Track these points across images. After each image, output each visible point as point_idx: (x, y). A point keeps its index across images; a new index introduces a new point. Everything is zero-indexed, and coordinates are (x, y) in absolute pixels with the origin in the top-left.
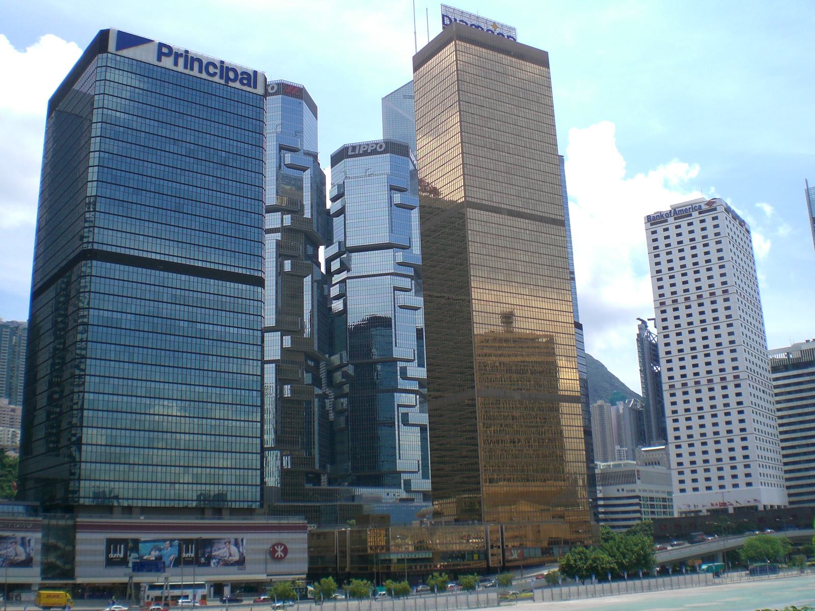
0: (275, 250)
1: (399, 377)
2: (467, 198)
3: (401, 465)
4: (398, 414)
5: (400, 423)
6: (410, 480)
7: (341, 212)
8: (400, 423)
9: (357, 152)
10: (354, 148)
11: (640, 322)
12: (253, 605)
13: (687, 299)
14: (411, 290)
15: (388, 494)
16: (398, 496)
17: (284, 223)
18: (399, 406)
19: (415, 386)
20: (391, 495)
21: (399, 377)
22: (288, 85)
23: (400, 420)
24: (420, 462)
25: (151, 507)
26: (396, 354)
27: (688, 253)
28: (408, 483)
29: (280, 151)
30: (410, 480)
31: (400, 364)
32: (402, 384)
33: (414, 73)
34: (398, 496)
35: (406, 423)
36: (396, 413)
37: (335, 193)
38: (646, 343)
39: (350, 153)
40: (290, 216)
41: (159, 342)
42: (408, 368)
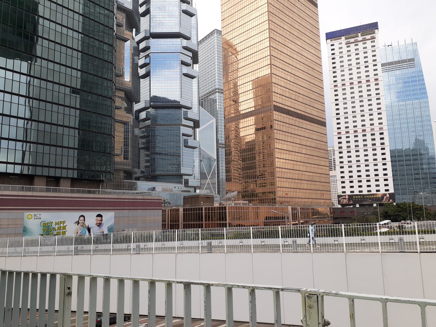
7: (147, 12)
12: (23, 150)
13: (355, 131)
14: (192, 136)
15: (175, 188)
18: (183, 135)
20: (177, 188)
25: (14, 174)
26: (183, 171)
27: (357, 104)
28: (187, 182)
30: (188, 180)
31: (183, 110)
41: (65, 159)
42: (189, 180)
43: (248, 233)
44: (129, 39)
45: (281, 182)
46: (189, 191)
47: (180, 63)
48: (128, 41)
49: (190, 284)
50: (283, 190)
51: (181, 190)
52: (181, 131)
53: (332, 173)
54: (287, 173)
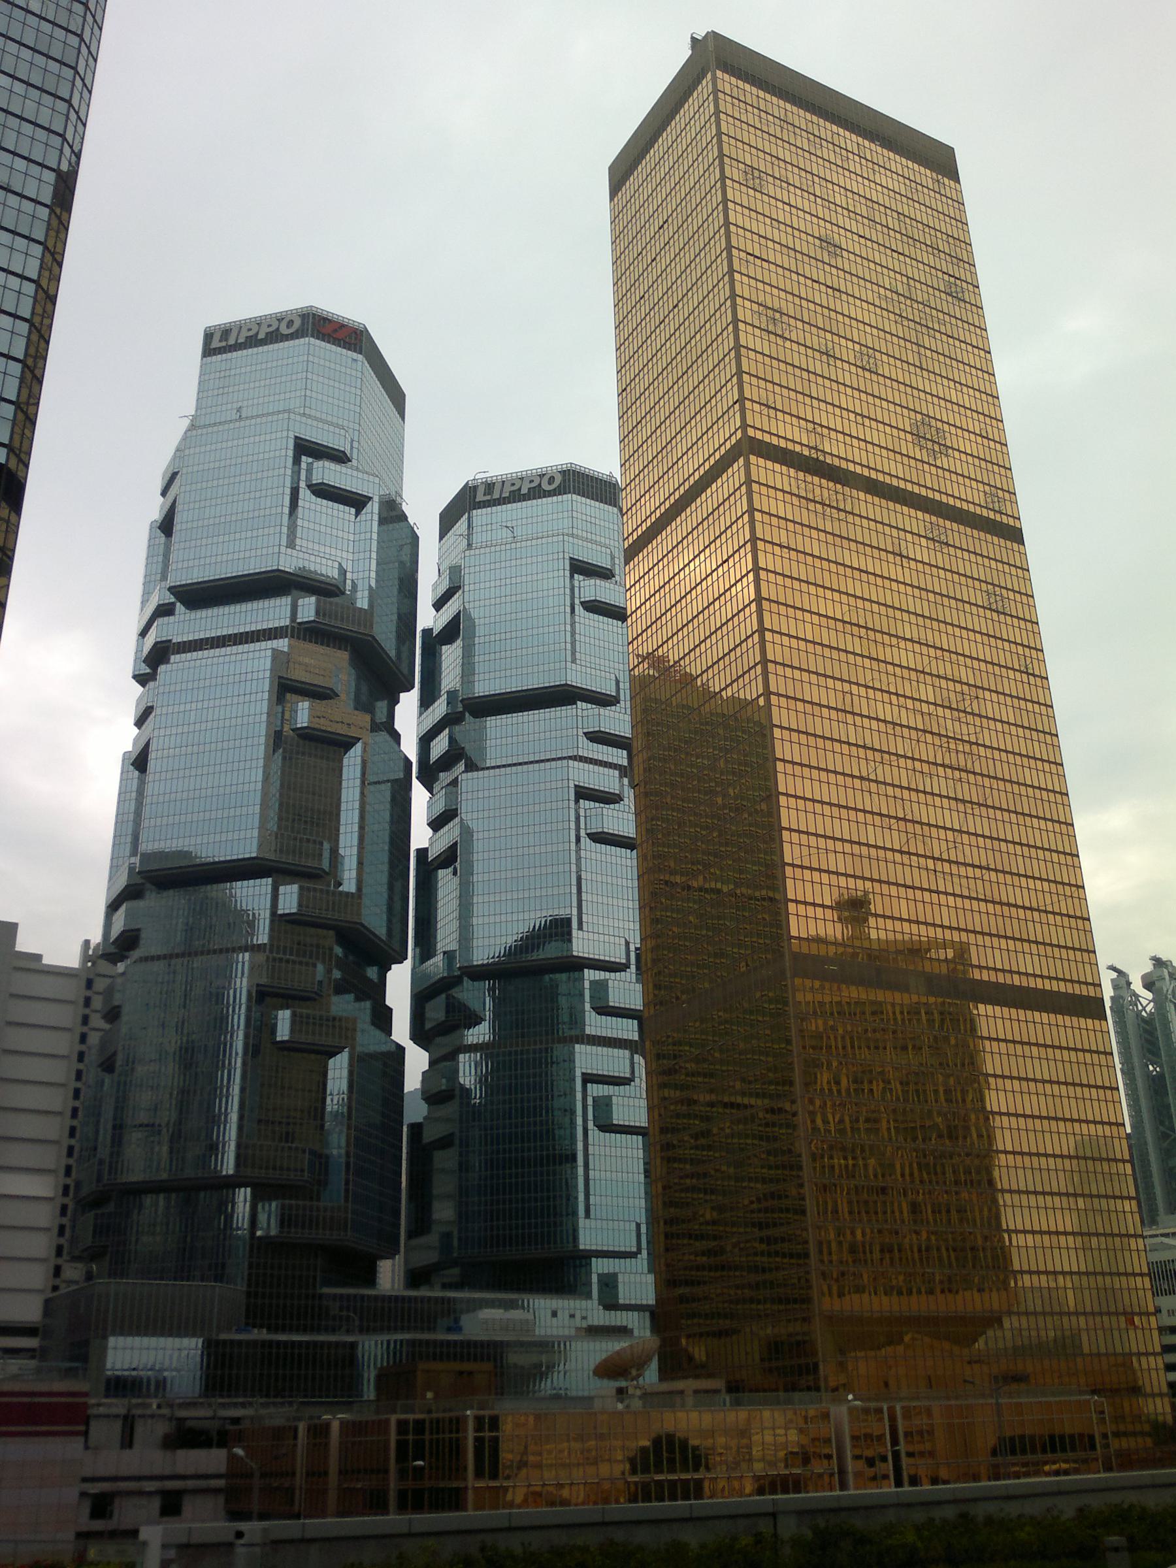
0: (344, 784)
1: (587, 1006)
2: (751, 432)
3: (589, 1236)
4: (582, 1099)
5: (591, 1125)
6: (614, 1276)
8: (591, 1125)
9: (496, 495)
10: (489, 486)
11: (1114, 975)
15: (554, 1314)
16: (584, 1318)
17: (299, 615)
18: (588, 1079)
19: (628, 1029)
20: (563, 1316)
21: (587, 1006)
22: (325, 319)
23: (590, 1116)
24: (643, 1229)
28: (609, 1283)
29: (297, 461)
30: (615, 1275)
31: (590, 975)
32: (595, 1024)
33: (611, 199)
34: (584, 1318)
35: (607, 1127)
36: (579, 1096)
37: (444, 586)
38: (1130, 1017)
39: (480, 497)
40: (313, 599)
42: (620, 1277)
43: (222, 1019)
44: (359, 739)
45: (1050, 1212)
46: (623, 1331)
47: (567, 567)
48: (354, 744)
49: (590, 1257)
50: (1111, 1246)
51: (584, 1325)
52: (577, 1064)
53: (265, 1331)
54: (1053, 1174)
